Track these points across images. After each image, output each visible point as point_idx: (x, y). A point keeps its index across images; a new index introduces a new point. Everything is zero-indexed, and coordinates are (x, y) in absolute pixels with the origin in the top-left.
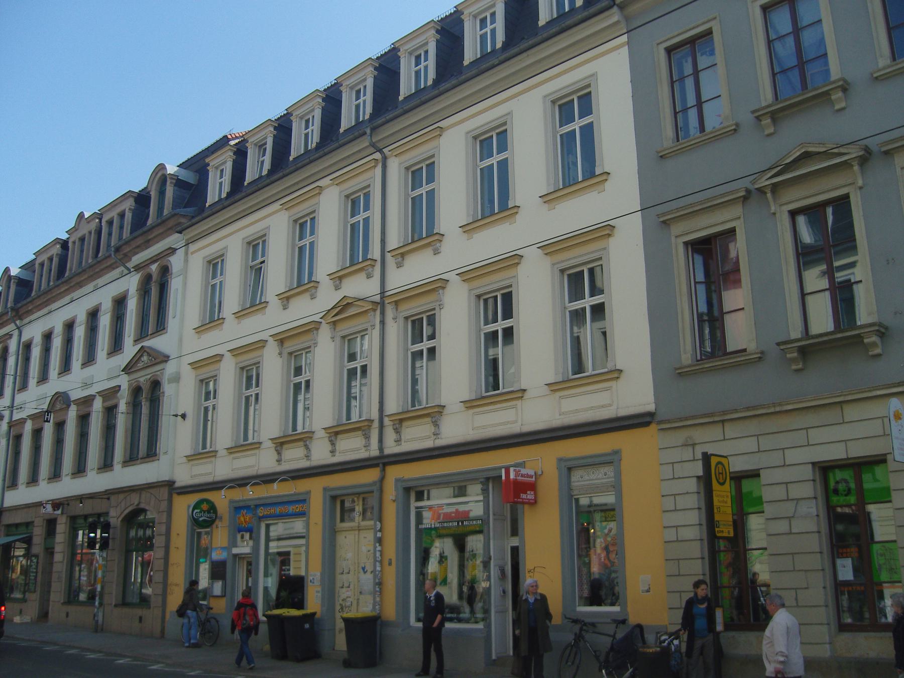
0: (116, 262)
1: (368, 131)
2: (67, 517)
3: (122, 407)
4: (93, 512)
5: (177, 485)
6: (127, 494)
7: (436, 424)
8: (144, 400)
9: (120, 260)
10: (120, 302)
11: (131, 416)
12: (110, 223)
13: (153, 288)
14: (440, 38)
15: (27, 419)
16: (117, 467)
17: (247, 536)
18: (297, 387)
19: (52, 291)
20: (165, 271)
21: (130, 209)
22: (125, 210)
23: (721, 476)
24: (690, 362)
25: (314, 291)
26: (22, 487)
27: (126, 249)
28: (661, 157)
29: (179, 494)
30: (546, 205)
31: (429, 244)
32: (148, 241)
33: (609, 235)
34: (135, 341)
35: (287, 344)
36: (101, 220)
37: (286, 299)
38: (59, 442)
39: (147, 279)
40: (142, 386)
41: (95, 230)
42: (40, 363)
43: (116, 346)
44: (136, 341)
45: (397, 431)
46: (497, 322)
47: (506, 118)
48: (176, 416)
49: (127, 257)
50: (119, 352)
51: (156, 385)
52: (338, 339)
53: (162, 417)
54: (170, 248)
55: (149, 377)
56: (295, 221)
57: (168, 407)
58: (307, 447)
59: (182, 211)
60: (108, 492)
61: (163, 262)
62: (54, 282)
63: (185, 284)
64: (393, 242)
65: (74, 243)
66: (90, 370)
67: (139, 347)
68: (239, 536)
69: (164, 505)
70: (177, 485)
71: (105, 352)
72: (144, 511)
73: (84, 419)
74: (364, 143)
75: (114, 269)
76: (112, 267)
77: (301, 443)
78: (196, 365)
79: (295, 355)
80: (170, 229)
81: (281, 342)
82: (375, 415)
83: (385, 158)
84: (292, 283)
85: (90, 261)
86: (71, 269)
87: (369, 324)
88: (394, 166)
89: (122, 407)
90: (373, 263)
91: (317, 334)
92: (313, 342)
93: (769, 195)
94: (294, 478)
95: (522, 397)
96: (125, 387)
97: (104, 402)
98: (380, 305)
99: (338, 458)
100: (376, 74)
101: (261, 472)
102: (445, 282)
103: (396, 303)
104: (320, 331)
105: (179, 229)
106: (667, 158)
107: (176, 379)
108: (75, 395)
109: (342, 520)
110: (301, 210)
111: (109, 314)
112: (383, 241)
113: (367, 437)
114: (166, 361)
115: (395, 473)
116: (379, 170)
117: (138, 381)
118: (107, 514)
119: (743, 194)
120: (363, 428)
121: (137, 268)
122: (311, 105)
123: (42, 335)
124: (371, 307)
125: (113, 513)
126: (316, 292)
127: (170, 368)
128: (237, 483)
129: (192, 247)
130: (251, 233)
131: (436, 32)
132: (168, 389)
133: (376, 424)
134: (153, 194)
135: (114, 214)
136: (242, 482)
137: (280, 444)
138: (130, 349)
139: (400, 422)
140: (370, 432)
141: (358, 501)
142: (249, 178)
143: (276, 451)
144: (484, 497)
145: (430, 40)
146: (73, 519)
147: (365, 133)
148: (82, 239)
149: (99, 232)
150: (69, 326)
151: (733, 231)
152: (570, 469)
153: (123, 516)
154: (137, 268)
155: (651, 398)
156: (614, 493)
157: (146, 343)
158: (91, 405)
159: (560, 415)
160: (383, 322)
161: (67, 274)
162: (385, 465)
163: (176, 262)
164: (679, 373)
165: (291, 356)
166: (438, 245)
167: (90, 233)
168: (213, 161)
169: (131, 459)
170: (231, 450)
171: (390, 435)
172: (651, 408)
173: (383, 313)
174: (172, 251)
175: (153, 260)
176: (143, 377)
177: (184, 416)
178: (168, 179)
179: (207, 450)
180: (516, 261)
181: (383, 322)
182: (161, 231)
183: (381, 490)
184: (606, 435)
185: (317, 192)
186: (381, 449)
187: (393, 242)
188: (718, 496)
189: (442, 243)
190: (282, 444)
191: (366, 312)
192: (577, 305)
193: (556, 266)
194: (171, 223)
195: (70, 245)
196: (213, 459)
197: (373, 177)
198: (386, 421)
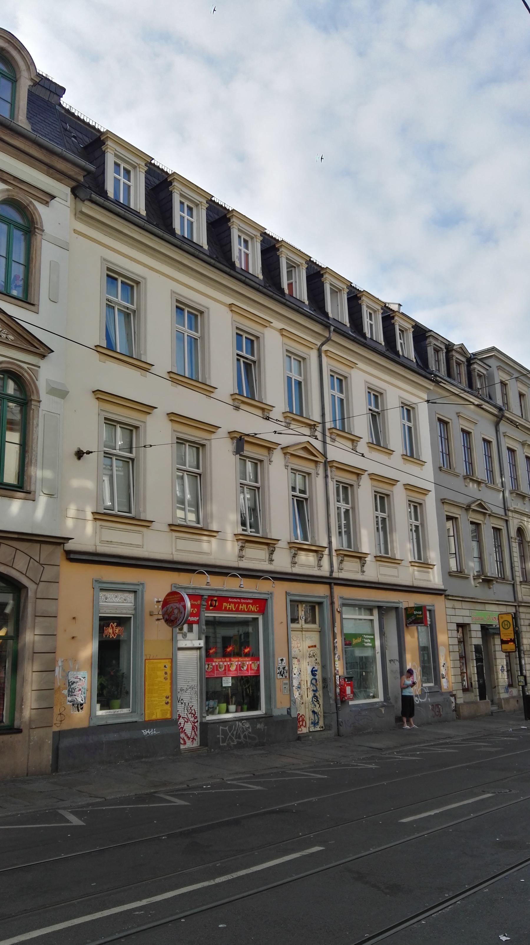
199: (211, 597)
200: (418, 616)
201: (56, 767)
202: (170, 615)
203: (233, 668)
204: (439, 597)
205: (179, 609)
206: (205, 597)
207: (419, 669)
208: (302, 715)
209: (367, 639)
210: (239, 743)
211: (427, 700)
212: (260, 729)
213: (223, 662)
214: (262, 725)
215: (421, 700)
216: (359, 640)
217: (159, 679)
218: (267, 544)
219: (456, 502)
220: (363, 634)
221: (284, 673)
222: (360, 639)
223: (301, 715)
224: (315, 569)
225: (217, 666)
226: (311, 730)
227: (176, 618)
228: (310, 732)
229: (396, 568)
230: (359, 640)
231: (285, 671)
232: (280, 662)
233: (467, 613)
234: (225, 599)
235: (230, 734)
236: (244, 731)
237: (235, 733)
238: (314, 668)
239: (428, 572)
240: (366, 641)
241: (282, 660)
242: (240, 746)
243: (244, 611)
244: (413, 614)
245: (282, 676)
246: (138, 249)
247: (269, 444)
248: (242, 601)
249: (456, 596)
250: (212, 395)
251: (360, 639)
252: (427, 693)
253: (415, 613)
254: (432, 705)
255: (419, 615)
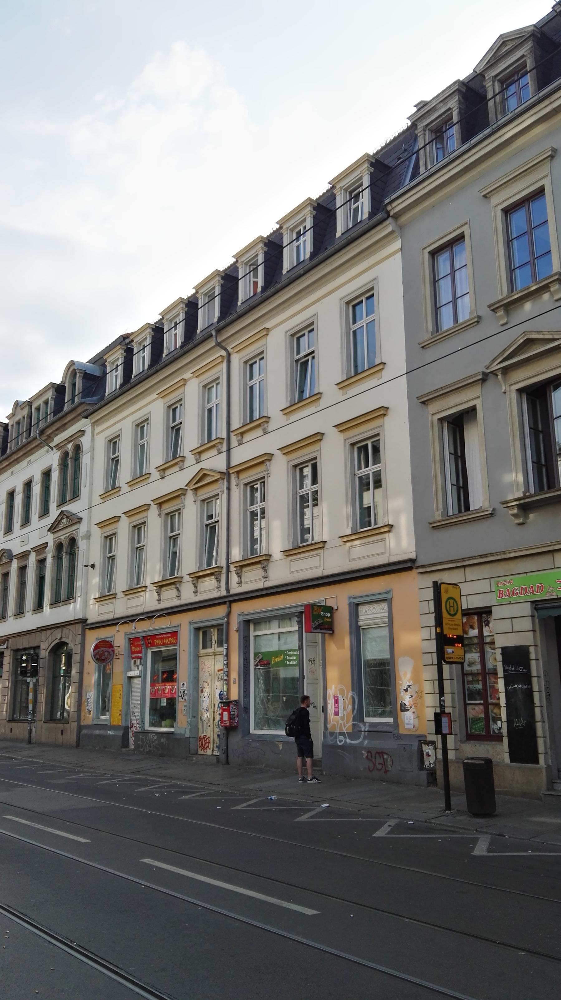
0: (41, 443)
1: (214, 333)
2: (11, 650)
3: (49, 561)
4: (29, 646)
5: (89, 622)
6: (53, 630)
7: (265, 569)
8: (64, 554)
9: (44, 441)
10: (47, 474)
11: (56, 567)
12: (38, 409)
13: (69, 463)
14: (268, 250)
15: (30, 551)
16: (46, 608)
17: (138, 662)
18: (254, 514)
19: (26, 447)
20: (78, 448)
21: (52, 398)
22: (48, 399)
23: (452, 609)
24: (440, 518)
25: (181, 464)
26: (10, 620)
27: (49, 431)
28: (423, 347)
29: (90, 629)
30: (341, 391)
31: (176, 464)
32: (65, 424)
33: (384, 415)
34: (58, 506)
35: (164, 506)
36: (31, 406)
37: (163, 470)
38: (22, 584)
39: (66, 454)
40: (63, 542)
41: (28, 415)
42: (41, 499)
43: (45, 512)
44: (59, 506)
45: (239, 575)
46: (303, 488)
47: (313, 318)
48: (87, 566)
49: (50, 438)
50: (47, 515)
51: (73, 541)
52: (199, 503)
53: (77, 568)
54: (80, 431)
55: (68, 535)
56: (169, 407)
57: (81, 561)
58: (265, 569)
59: (87, 400)
60: (39, 629)
61: (77, 442)
62: (26, 438)
63: (93, 459)
64: (236, 424)
65: (12, 426)
66: (27, 530)
67: (59, 511)
68: (132, 662)
69: (79, 638)
70: (89, 622)
71: (37, 515)
72: (66, 644)
73: (23, 569)
74: (211, 343)
75: (41, 447)
76: (39, 447)
77: (173, 586)
78: (102, 525)
79: (171, 515)
80: (80, 414)
81: (160, 505)
82: (224, 563)
83: (229, 355)
84: (245, 419)
85: (24, 440)
86: (10, 448)
87: (220, 490)
88: (236, 360)
89: (49, 561)
90: (221, 441)
91: (185, 498)
92: (267, 472)
93: (500, 377)
94: (169, 614)
95: (324, 547)
96: (51, 544)
97: (37, 556)
98: (226, 475)
99: (199, 598)
100: (315, 214)
101: (147, 610)
102: (271, 455)
103: (238, 473)
104: (187, 496)
105: (84, 414)
106: (427, 348)
107: (88, 536)
108: (17, 550)
109: (204, 647)
110: (172, 398)
111: (39, 484)
112: (229, 424)
113: (219, 580)
114: (80, 522)
115: (238, 608)
116: (225, 364)
117: (60, 539)
118: (38, 647)
119: (480, 377)
120: (216, 574)
121: (58, 447)
122: (176, 310)
123: (7, 493)
124: (219, 477)
125: (43, 646)
126: (268, 427)
127: (83, 528)
128: (166, 612)
129: (98, 430)
130: (139, 417)
131: (371, 166)
132: (82, 544)
133: (224, 570)
134: (67, 385)
135: (40, 402)
136: (131, 619)
137: (161, 586)
138: (54, 513)
139: (242, 567)
140: (220, 577)
141: (214, 632)
142: (135, 372)
143: (194, 584)
144: (299, 628)
145: (307, 217)
146: (16, 651)
147: (211, 336)
148: (18, 423)
149: (30, 416)
150: (28, 485)
151: (473, 409)
152: (357, 605)
153: (50, 648)
154: (58, 447)
155: (413, 548)
156: (388, 625)
157: (65, 508)
158: (28, 559)
159: (350, 561)
160: (229, 489)
161: (8, 452)
162: (231, 602)
163: (85, 441)
164: (433, 527)
165: (168, 517)
166: (266, 425)
167: (24, 417)
168: (110, 359)
169: (55, 602)
170: (127, 593)
171: (234, 579)
172: (413, 556)
173: (229, 482)
174: (82, 432)
175: (68, 440)
176: (63, 536)
177: (93, 566)
178: (77, 373)
179: (258, 555)
180: (319, 438)
181: (229, 489)
182: (7, 463)
183: (228, 623)
184: (241, 602)
185: (183, 383)
186: (228, 590)
187: (236, 424)
188: (447, 624)
189: (269, 424)
190: (161, 586)
191: (216, 481)
192: (364, 471)
193: (347, 441)
194: (80, 410)
195: (10, 428)
196: (113, 600)
197: (221, 371)
198: (232, 569)
199: (145, 638)
200: (326, 619)
201: (78, 745)
202: (101, 655)
203: (167, 691)
204: (410, 572)
205: (109, 652)
206: (141, 638)
207: (350, 694)
208: (209, 737)
209: (291, 656)
210: (150, 751)
211: (362, 742)
212: (163, 743)
213: (161, 686)
214: (165, 740)
215: (348, 741)
216: (280, 658)
217: (117, 699)
218: (173, 583)
219: (445, 387)
220: (286, 651)
221: (184, 696)
222: (282, 657)
223: (207, 737)
224: (215, 592)
225: (157, 689)
226: (214, 754)
227: (106, 658)
228: (212, 755)
229: (318, 555)
230: (280, 658)
231: (185, 695)
232: (182, 686)
233: (484, 586)
234: (154, 637)
235: (145, 743)
236: (153, 742)
237: (148, 742)
238: (221, 691)
239: (383, 540)
240: (290, 658)
241: (183, 684)
242: (149, 753)
243: (168, 644)
244: (319, 616)
245: (183, 698)
246: (119, 413)
247: (253, 461)
248: (165, 636)
249: (432, 565)
250: (121, 493)
251: (282, 657)
252: (365, 731)
253: (323, 614)
254: (369, 752)
255: (327, 617)
